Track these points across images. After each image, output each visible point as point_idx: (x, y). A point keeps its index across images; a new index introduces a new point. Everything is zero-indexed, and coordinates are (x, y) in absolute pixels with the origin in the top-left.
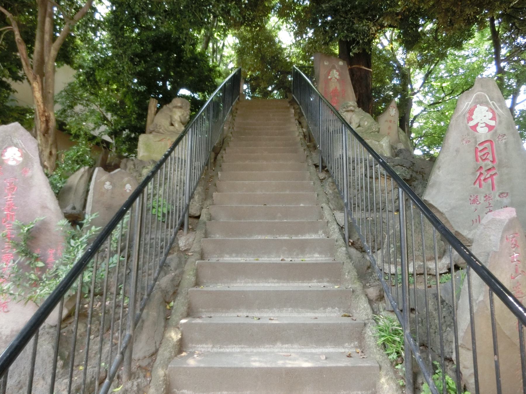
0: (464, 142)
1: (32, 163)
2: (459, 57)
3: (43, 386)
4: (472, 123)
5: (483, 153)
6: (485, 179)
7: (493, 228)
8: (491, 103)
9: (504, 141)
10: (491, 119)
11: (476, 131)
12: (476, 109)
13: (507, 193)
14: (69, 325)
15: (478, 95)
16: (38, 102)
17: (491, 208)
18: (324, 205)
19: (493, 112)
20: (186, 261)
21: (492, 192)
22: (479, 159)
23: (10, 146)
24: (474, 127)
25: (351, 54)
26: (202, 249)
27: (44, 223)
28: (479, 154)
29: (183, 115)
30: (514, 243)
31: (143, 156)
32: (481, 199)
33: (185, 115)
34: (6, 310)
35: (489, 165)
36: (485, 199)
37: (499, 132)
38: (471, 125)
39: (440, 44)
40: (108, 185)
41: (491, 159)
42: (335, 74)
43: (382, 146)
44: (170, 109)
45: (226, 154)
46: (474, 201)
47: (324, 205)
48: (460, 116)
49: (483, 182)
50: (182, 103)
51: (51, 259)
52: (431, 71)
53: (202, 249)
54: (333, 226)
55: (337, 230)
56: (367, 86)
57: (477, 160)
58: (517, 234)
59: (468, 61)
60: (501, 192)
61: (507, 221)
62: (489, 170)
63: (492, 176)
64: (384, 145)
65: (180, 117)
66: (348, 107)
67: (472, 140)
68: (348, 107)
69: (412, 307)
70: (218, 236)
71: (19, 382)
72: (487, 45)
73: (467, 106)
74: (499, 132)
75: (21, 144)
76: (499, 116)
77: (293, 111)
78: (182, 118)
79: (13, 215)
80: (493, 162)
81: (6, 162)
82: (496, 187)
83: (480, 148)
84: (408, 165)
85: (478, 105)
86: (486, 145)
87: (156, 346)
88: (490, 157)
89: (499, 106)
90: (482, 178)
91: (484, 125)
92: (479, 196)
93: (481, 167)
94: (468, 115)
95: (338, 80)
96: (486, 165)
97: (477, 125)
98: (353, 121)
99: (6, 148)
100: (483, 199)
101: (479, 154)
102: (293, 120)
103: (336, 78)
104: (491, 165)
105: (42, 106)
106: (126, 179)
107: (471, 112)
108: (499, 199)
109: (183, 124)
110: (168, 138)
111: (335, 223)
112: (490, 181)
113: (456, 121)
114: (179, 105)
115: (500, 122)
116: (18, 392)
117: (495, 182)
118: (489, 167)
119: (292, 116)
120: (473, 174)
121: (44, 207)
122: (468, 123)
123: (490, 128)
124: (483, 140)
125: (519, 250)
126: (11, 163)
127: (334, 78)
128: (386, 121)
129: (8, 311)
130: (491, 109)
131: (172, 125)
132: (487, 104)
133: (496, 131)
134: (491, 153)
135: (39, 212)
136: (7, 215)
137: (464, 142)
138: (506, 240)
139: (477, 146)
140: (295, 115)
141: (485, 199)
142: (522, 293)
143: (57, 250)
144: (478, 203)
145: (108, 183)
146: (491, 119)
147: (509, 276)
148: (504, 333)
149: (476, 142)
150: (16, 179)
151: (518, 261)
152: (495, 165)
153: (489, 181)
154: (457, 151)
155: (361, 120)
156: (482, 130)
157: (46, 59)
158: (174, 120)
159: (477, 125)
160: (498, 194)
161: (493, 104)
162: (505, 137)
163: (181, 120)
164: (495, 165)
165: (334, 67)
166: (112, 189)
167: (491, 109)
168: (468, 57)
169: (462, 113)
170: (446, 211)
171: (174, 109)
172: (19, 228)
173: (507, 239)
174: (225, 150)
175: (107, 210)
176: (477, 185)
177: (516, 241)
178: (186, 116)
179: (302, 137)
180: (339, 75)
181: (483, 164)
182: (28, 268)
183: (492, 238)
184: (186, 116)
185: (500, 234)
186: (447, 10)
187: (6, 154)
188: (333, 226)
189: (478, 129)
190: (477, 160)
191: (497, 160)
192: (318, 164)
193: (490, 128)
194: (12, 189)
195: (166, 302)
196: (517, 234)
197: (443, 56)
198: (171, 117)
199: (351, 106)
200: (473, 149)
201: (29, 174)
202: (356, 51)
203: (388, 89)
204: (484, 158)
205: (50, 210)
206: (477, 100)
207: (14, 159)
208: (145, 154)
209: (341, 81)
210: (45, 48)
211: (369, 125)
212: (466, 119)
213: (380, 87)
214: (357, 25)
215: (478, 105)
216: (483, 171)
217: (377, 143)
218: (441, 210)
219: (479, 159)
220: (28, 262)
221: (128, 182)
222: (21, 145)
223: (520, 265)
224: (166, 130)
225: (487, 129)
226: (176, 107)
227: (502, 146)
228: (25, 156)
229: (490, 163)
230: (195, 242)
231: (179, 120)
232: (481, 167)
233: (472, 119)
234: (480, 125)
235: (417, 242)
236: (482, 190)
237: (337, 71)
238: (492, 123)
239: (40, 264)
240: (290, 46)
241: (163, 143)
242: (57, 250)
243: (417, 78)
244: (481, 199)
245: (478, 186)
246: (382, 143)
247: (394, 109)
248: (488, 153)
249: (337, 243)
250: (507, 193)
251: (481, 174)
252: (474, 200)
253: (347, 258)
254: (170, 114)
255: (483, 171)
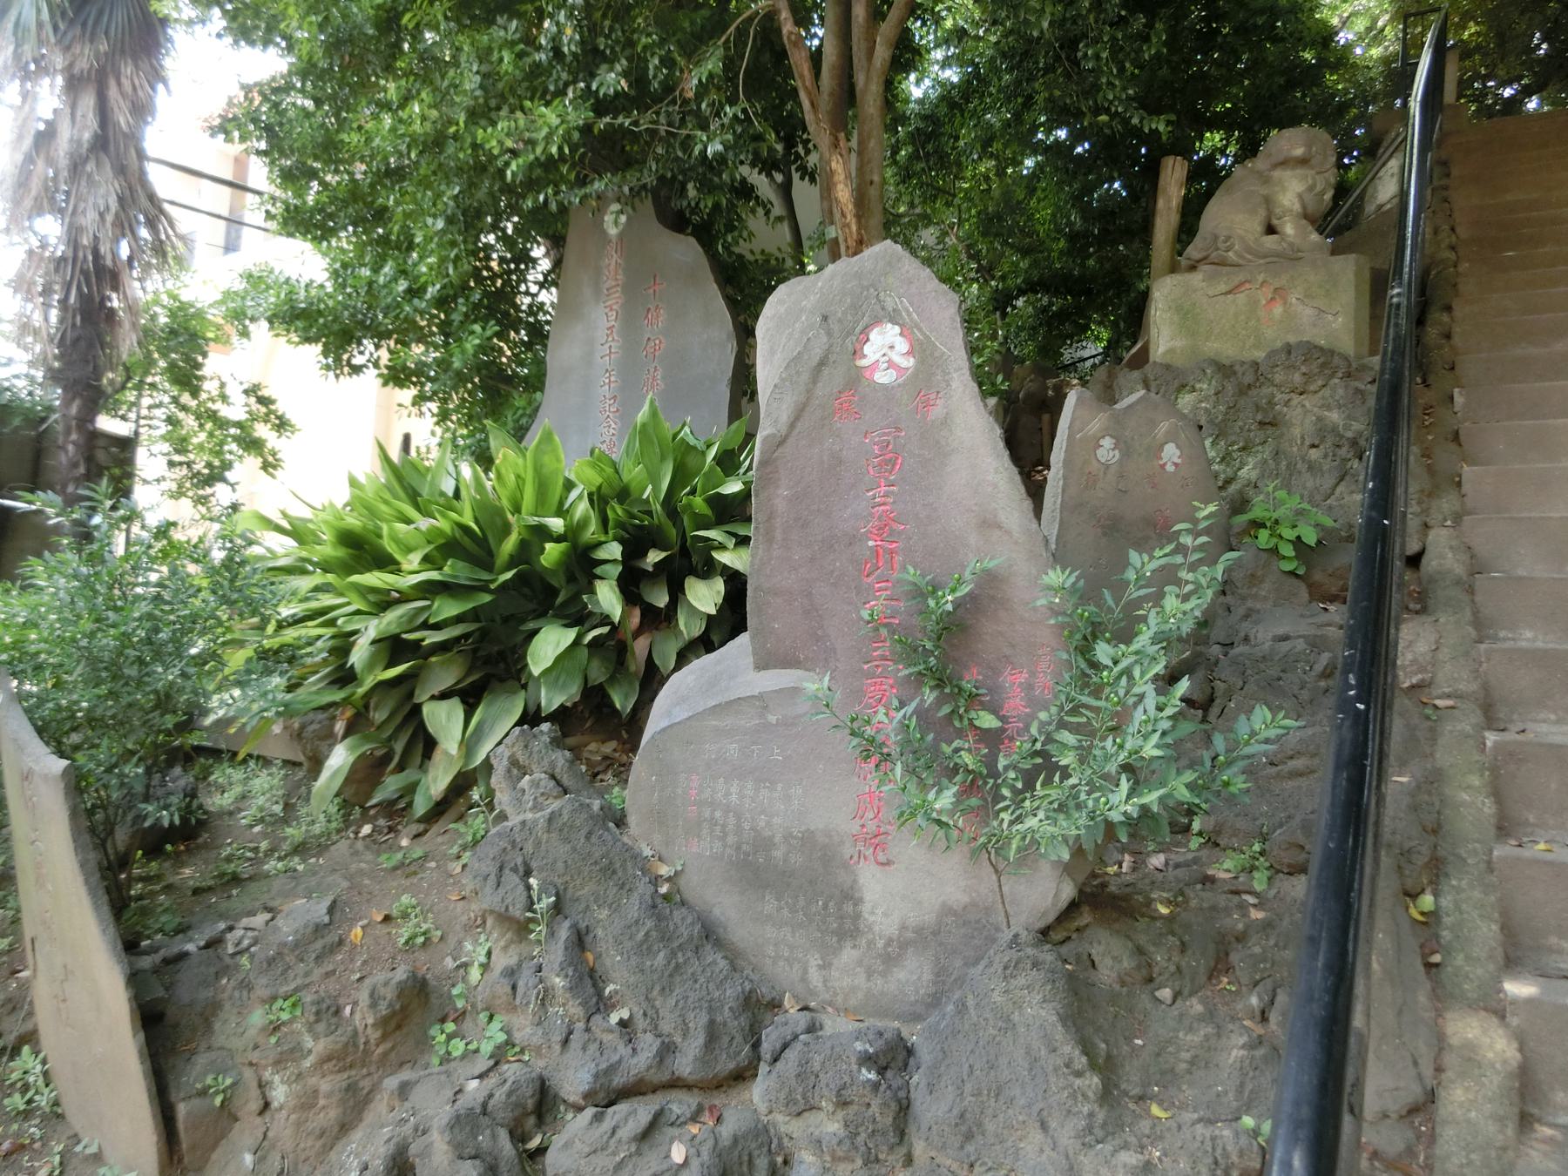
1: (946, 373)
3: (1042, 1151)
14: (1074, 936)
16: (843, 215)
20: (1433, 735)
23: (876, 321)
26: (1486, 687)
27: (990, 580)
29: (1311, 189)
31: (1171, 351)
33: (1319, 188)
34: (881, 857)
40: (1107, 450)
44: (1260, 174)
45: (1468, 319)
50: (1309, 146)
51: (1015, 704)
53: (1486, 687)
65: (1300, 196)
70: (1529, 634)
71: (962, 1116)
75: (907, 311)
78: (1308, 198)
79: (891, 552)
81: (867, 374)
87: (1420, 1077)
99: (866, 331)
105: (854, 228)
106: (1164, 426)
109: (1312, 221)
110: (1261, 278)
114: (1299, 152)
116: (962, 1147)
121: (988, 524)
126: (883, 377)
129: (888, 863)
131: (1271, 230)
135: (973, 539)
136: (876, 552)
143: (1033, 674)
145: (1107, 442)
150: (898, 429)
157: (860, 79)
158: (1277, 211)
163: (1304, 207)
166: (1120, 461)
171: (1277, 174)
172: (919, 594)
174: (1448, 308)
175: (1105, 534)
178: (1323, 193)
182: (949, 727)
184: (1323, 193)
187: (867, 349)
194: (889, 463)
195: (1407, 894)
198: (1268, 201)
201: (937, 411)
205: (1008, 533)
207: (891, 364)
208: (1179, 343)
210: (855, 48)
220: (946, 710)
221: (1171, 437)
222: (909, 314)
224: (1249, 250)
226: (1285, 163)
228: (921, 349)
230: (1444, 654)
231: (1297, 207)
239: (987, 721)
241: (1241, 298)
242: (1033, 674)
254: (1264, 191)
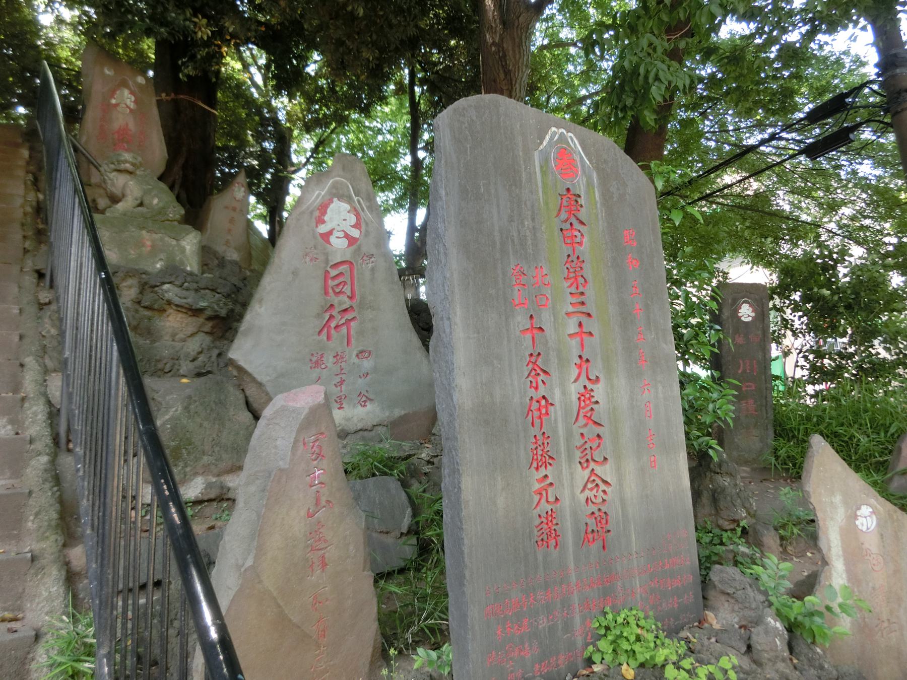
0: (308, 259)
2: (370, 128)
4: (322, 229)
5: (337, 282)
6: (337, 327)
7: (283, 425)
8: (356, 199)
9: (370, 265)
10: (352, 226)
11: (328, 242)
12: (332, 206)
13: (370, 352)
15: (337, 182)
17: (344, 377)
18: (30, 361)
19: (358, 216)
21: (347, 350)
22: (331, 291)
24: (326, 236)
25: (181, 75)
28: (331, 283)
30: (317, 451)
32: (329, 360)
35: (345, 303)
36: (335, 360)
37: (364, 249)
38: (322, 231)
39: (338, 100)
41: (349, 294)
42: (126, 98)
43: (183, 250)
46: (317, 364)
47: (30, 361)
48: (303, 213)
49: (333, 332)
52: (324, 140)
54: (35, 408)
55: (42, 417)
56: (206, 140)
57: (326, 293)
58: (322, 434)
59: (380, 138)
60: (360, 348)
61: (306, 411)
62: (345, 310)
63: (348, 321)
64: (188, 248)
66: (119, 162)
67: (322, 258)
68: (119, 162)
69: (158, 577)
72: (405, 122)
73: (317, 197)
74: (364, 249)
76: (367, 224)
77: (25, 153)
80: (351, 298)
82: (353, 341)
83: (333, 273)
84: (227, 290)
85: (335, 200)
86: (342, 268)
88: (347, 289)
89: (368, 208)
90: (333, 325)
91: (342, 234)
92: (325, 356)
93: (332, 305)
94: (317, 213)
95: (131, 110)
96: (340, 303)
97: (330, 233)
98: (128, 192)
100: (332, 360)
101: (331, 283)
102: (21, 173)
103: (127, 107)
104: (347, 303)
107: (323, 208)
108: (356, 360)
111: (42, 401)
112: (345, 331)
113: (298, 220)
115: (367, 234)
117: (352, 332)
118: (344, 307)
119: (22, 163)
120: (319, 316)
122: (317, 226)
123: (352, 241)
124: (339, 260)
125: (325, 463)
127: (127, 107)
128: (226, 207)
130: (355, 210)
132: (349, 200)
133: (359, 248)
134: (349, 283)
137: (308, 259)
138: (302, 447)
139: (329, 269)
140: (28, 163)
141: (335, 360)
142: (325, 541)
144: (323, 366)
146: (352, 226)
147: (303, 513)
148: (290, 620)
149: (327, 261)
151: (321, 483)
152: (355, 304)
153: (344, 330)
154: (295, 273)
155: (146, 192)
156: (338, 242)
159: (330, 233)
160: (355, 353)
161: (359, 202)
162: (373, 259)
164: (355, 304)
165: (124, 84)
167: (355, 210)
168: (380, 131)
169: (308, 208)
170: (268, 381)
173: (304, 444)
176: (324, 336)
177: (320, 447)
179: (29, 209)
180: (136, 102)
181: (336, 300)
183: (279, 443)
185: (294, 435)
186: (340, 43)
188: (35, 408)
189: (333, 239)
190: (326, 293)
191: (358, 297)
192: (43, 271)
193: (352, 241)
196: (322, 434)
197: (342, 120)
199: (126, 161)
200: (321, 273)
202: (190, 70)
203: (251, 155)
204: (338, 290)
206: (334, 191)
209: (139, 112)
211: (161, 205)
212: (314, 220)
213: (236, 147)
214: (173, 15)
215: (335, 200)
216: (334, 313)
217: (174, 242)
218: (259, 378)
219: (331, 291)
223: (325, 491)
225: (345, 242)
227: (368, 275)
229: (346, 299)
232: (332, 305)
233: (323, 222)
234: (336, 234)
235: (211, 439)
236: (331, 344)
237: (132, 93)
238: (355, 233)
240: (692, 245)
243: (302, 146)
244: (329, 360)
245: (325, 338)
246: (183, 243)
247: (243, 189)
248: (345, 283)
249: (33, 447)
250: (370, 352)
251: (331, 317)
252: (317, 362)
253: (45, 481)
255: (334, 313)
